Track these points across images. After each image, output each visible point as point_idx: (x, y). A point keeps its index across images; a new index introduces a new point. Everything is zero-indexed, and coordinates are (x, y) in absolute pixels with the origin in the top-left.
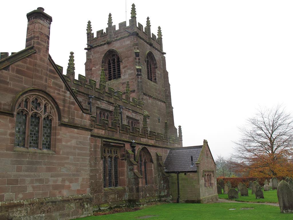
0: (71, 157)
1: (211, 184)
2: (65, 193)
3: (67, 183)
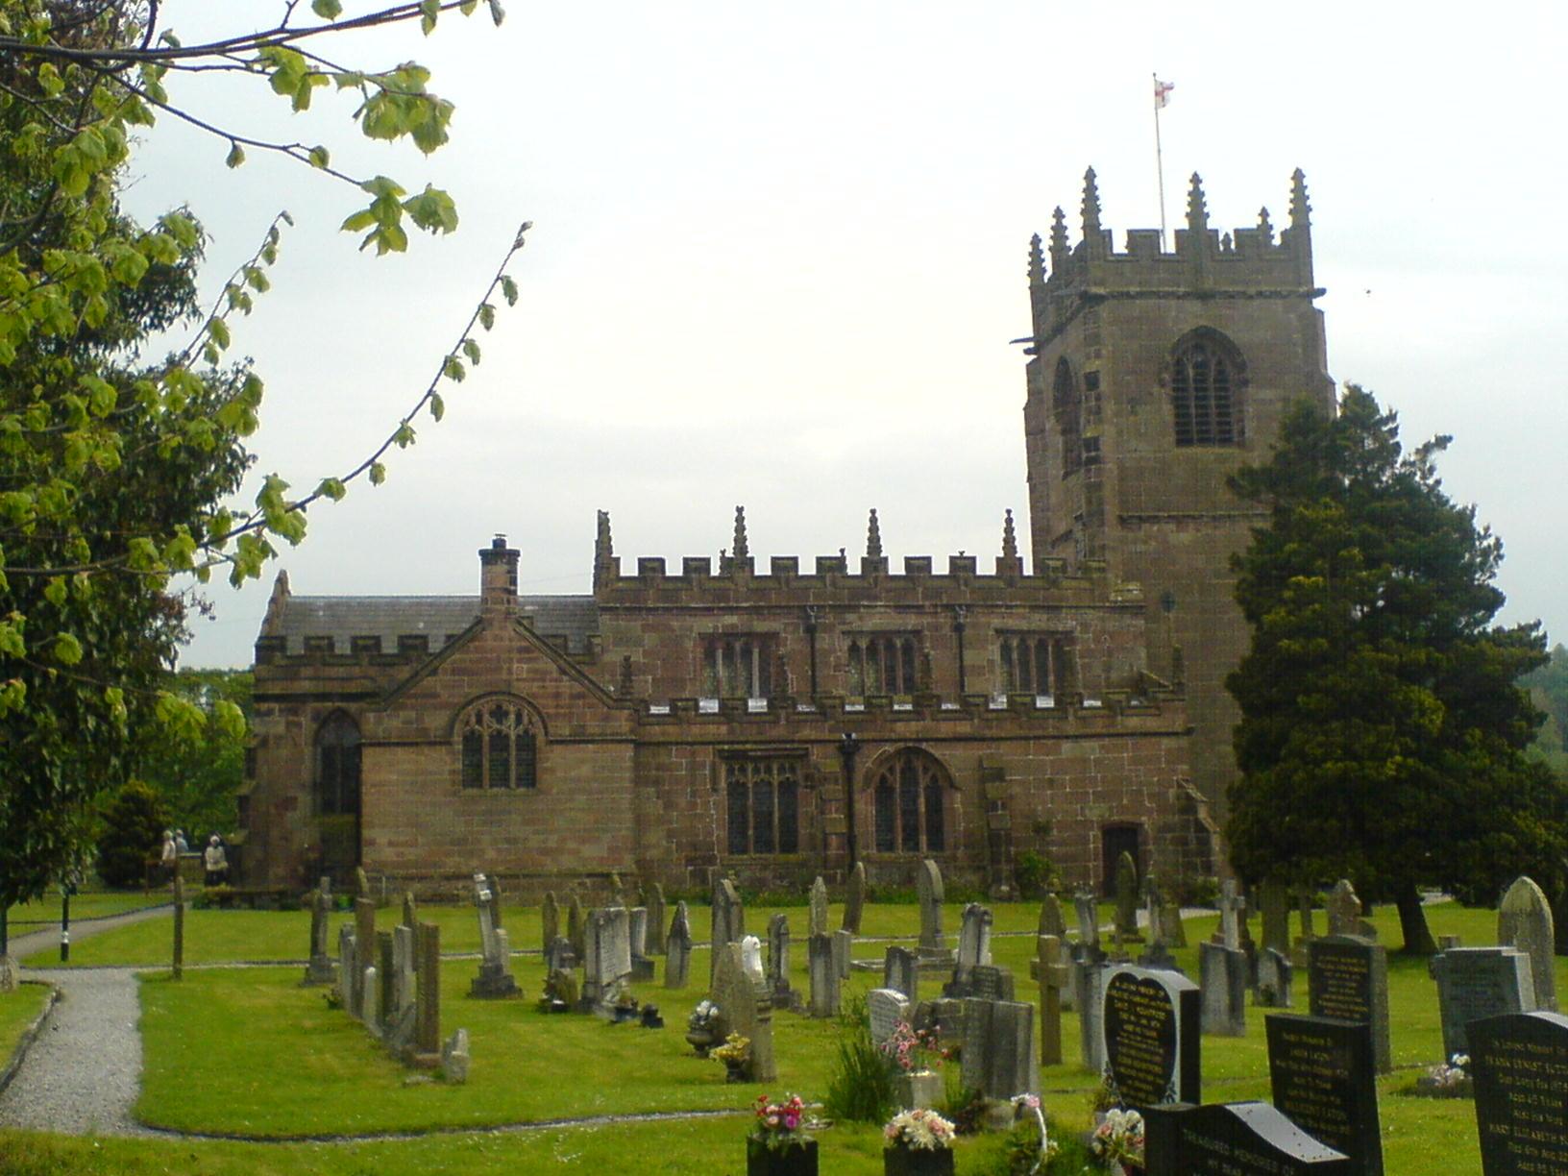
0: (583, 798)
1: (599, 838)
2: (568, 862)
3: (571, 845)
